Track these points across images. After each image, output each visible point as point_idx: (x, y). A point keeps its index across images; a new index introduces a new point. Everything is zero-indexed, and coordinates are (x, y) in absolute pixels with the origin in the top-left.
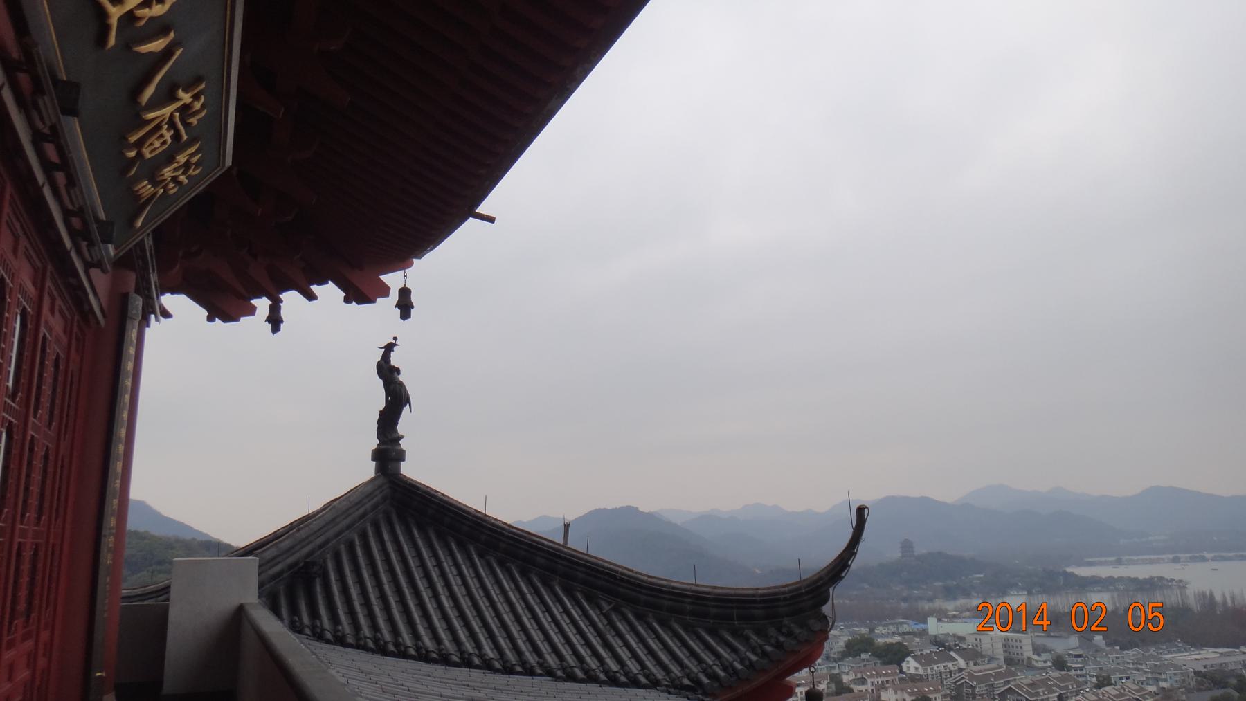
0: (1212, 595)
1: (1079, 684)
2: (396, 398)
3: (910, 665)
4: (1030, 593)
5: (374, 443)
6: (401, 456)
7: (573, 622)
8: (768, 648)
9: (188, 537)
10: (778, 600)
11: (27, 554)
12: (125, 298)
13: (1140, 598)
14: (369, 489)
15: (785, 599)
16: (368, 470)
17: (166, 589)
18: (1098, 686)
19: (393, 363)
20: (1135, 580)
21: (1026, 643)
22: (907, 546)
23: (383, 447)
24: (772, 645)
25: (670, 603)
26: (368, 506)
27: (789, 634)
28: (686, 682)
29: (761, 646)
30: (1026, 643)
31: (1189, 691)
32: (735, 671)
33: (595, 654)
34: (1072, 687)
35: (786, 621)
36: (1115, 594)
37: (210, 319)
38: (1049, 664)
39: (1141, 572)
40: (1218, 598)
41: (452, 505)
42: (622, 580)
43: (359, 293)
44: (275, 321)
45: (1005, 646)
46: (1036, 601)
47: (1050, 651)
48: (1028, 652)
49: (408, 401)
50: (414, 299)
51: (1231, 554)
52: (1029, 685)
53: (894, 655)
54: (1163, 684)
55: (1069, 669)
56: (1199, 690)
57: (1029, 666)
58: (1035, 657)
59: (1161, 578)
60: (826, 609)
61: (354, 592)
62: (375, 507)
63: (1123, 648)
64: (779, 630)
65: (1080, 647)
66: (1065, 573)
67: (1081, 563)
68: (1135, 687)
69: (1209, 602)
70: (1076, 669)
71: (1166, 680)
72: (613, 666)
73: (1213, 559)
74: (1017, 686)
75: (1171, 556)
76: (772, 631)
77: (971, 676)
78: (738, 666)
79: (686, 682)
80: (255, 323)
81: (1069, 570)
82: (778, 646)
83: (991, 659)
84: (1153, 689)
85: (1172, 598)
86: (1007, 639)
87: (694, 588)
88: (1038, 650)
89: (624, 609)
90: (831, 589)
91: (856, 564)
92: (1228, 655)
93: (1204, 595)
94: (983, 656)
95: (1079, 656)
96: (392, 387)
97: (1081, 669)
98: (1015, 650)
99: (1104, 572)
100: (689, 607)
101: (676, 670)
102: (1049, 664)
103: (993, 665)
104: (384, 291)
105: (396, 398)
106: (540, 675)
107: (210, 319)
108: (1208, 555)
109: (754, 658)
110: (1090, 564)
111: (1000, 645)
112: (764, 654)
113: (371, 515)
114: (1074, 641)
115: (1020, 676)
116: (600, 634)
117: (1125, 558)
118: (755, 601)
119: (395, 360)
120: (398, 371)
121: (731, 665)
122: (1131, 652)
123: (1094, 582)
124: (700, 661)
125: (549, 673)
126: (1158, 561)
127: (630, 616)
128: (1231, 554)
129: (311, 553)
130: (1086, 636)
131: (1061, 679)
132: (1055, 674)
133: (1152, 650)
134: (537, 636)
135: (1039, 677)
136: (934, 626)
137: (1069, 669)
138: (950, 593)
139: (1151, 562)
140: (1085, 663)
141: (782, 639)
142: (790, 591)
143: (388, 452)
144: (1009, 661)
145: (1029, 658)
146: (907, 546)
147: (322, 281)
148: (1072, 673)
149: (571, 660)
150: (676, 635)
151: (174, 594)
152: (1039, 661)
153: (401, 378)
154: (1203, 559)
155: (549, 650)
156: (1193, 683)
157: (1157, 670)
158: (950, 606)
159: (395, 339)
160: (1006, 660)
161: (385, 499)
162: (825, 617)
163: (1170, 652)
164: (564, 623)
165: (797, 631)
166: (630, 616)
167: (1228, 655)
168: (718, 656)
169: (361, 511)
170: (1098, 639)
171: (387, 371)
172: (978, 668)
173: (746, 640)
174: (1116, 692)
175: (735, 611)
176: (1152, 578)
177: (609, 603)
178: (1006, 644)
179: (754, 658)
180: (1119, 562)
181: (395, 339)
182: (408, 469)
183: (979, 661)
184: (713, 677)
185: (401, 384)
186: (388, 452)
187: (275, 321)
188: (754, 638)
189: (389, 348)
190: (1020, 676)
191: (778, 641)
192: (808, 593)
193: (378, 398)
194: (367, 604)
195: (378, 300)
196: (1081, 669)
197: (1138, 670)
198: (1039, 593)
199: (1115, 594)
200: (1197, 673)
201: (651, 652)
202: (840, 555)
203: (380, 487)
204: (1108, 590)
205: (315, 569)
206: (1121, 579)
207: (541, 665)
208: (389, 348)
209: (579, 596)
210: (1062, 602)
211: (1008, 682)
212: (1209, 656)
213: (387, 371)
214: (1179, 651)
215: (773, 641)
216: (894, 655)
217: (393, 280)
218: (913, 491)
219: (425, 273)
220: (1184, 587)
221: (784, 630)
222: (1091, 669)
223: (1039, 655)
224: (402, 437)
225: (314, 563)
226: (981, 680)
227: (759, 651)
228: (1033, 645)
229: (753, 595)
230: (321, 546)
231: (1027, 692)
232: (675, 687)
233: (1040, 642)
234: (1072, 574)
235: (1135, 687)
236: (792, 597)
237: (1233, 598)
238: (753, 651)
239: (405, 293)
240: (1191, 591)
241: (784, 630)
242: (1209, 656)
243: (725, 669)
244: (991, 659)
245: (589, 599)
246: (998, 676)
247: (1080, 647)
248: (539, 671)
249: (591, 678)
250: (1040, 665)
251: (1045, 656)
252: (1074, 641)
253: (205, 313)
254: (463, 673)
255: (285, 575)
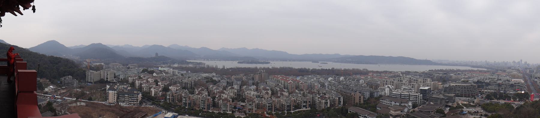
3: (155, 74)
22: (157, 54)
39: (198, 61)
48: (177, 73)
53: (152, 72)
57: (177, 75)
85: (203, 66)
99: (192, 61)
123: (190, 62)
130: (187, 71)
136: (160, 69)
138: (164, 63)
146: (157, 54)
157: (198, 76)
158: (164, 66)
210: (184, 66)
212: (207, 75)
216: (152, 72)
217: (32, 4)
218: (50, 40)
239: (34, 7)
242: (207, 75)
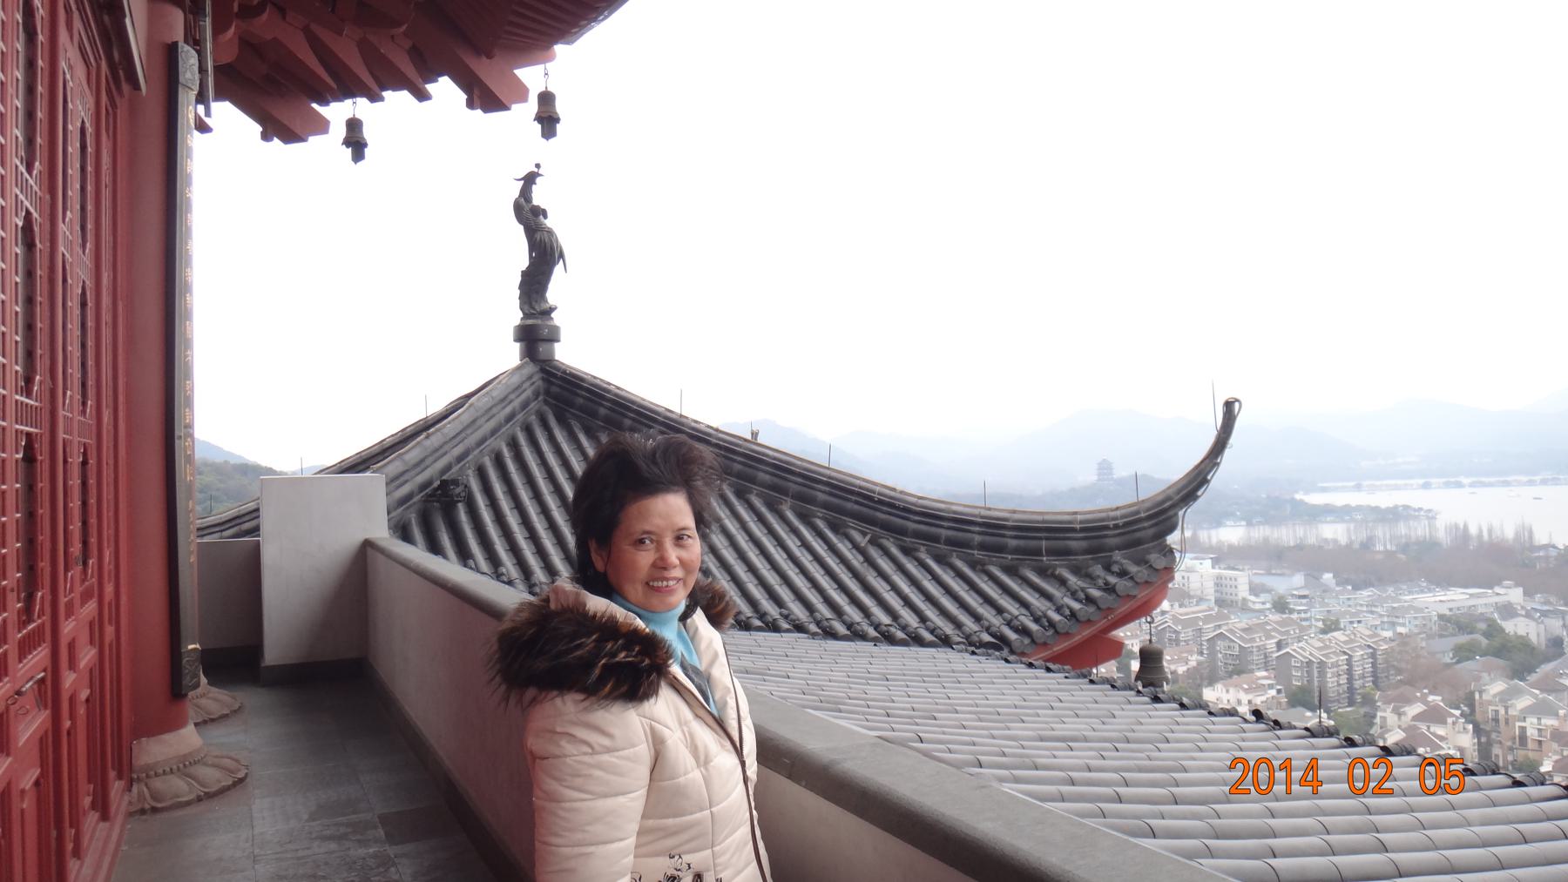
0: (1466, 526)
1: (1302, 629)
2: (544, 256)
4: (1250, 524)
5: (516, 317)
6: (553, 337)
7: (817, 559)
8: (1095, 593)
9: (219, 459)
10: (1106, 528)
11: (76, 460)
12: (171, 52)
13: (1381, 532)
14: (516, 380)
15: (1116, 527)
16: (509, 356)
17: (257, 510)
18: (1324, 632)
19: (535, 202)
20: (1376, 509)
21: (1241, 581)
23: (530, 322)
24: (1099, 588)
25: (950, 533)
26: (517, 403)
27: (1123, 574)
28: (986, 638)
29: (1083, 590)
30: (1241, 581)
31: (1430, 637)
32: (1052, 624)
33: (854, 601)
34: (1293, 631)
35: (1117, 556)
36: (1352, 526)
37: (266, 136)
38: (1268, 606)
40: (1473, 531)
41: (633, 402)
42: (881, 502)
43: (485, 98)
44: (355, 142)
45: (1217, 585)
46: (1260, 533)
47: (1269, 591)
48: (1243, 592)
49: (561, 256)
50: (560, 107)
51: (1492, 480)
52: (1244, 630)
54: (1400, 629)
55: (1291, 611)
56: (1441, 636)
57: (1244, 607)
58: (1252, 598)
59: (1406, 507)
60: (1173, 539)
61: (513, 520)
62: (525, 405)
63: (1356, 588)
64: (1107, 568)
65: (1305, 587)
66: (1293, 499)
67: (1307, 492)
68: (1368, 632)
69: (1462, 536)
70: (1299, 612)
71: (1403, 625)
72: (885, 619)
73: (1472, 485)
74: (1231, 631)
75: (1421, 481)
76: (1098, 570)
77: (1175, 619)
78: (1056, 617)
79: (986, 638)
80: (327, 147)
81: (1298, 497)
82: (1109, 589)
83: (1201, 600)
84: (1388, 634)
85: (1419, 530)
86: (1219, 577)
87: (984, 512)
88: (1255, 590)
89: (885, 542)
90: (1181, 513)
91: (1220, 479)
92: (1478, 596)
93: (1456, 526)
94: (1190, 597)
95: (1304, 597)
96: (538, 236)
97: (1305, 612)
98: (1229, 590)
99: (1338, 499)
100: (978, 538)
101: (969, 624)
102: (1268, 606)
103: (1203, 606)
104: (521, 93)
105: (544, 256)
106: (788, 631)
107: (266, 136)
108: (1466, 481)
109: (1076, 606)
110: (1324, 490)
111: (1211, 584)
112: (1090, 600)
113: (520, 417)
114: (1298, 580)
115: (1234, 619)
116: (856, 575)
117: (1365, 483)
118: (1073, 530)
119: (539, 197)
120: (544, 213)
121: (1045, 616)
122: (1365, 593)
123: (1328, 511)
124: (1000, 611)
125: (799, 628)
126: (1405, 487)
127: (895, 551)
128: (1492, 480)
129: (448, 468)
130: (1313, 575)
131: (1282, 623)
132: (1274, 617)
133: (1390, 589)
134: (772, 578)
135: (1255, 621)
137: (1291, 611)
139: (1397, 488)
140: (1311, 605)
141: (1112, 580)
142: (1123, 517)
143: (535, 335)
144: (1220, 602)
145: (1244, 599)
146: (1105, 468)
147: (432, 79)
148: (1295, 616)
149: (824, 611)
150: (960, 575)
151: (267, 523)
152: (1259, 602)
153: (549, 223)
154: (1459, 485)
155: (792, 597)
156: (1435, 628)
159: (538, 166)
160: (1217, 601)
161: (536, 394)
162: (1171, 551)
163: (1410, 593)
164: (803, 556)
165: (1133, 569)
166: (895, 551)
167: (1478, 596)
168: (1024, 604)
169: (508, 410)
170: (1328, 577)
171: (529, 215)
172: (1183, 610)
173: (1063, 582)
174: (1344, 638)
175: (1044, 543)
176: (1396, 507)
177: (864, 534)
178: (1218, 585)
179: (1076, 606)
180: (1358, 487)
181: (538, 166)
182: (569, 353)
183: (1186, 601)
184: (1023, 631)
185: (550, 232)
186: (535, 335)
187: (355, 142)
188: (1073, 580)
189: (530, 180)
190: (1234, 619)
191: (1107, 583)
192: (1150, 517)
193: (519, 256)
194: (533, 537)
195: (515, 107)
196: (1305, 612)
197: (1372, 612)
198: (1260, 523)
199: (1352, 526)
200: (1441, 617)
201: (929, 598)
202: (1197, 467)
203: (530, 378)
204: (1343, 521)
205: (458, 490)
206: (1359, 508)
207: (786, 617)
208: (530, 180)
209: (821, 524)
210: (1286, 535)
211: (1219, 626)
212: (1457, 598)
213: (529, 215)
214: (1422, 592)
215: (1101, 582)
217: (531, 76)
219: (568, 67)
220: (1434, 518)
221: (1115, 568)
222: (1317, 612)
223: (1256, 595)
224: (552, 309)
225: (455, 482)
226: (1187, 623)
227: (1082, 596)
228: (1250, 583)
229: (1070, 522)
230: (460, 459)
231: (1241, 638)
232: (971, 644)
233: (1257, 580)
234: (1302, 502)
235: (1368, 632)
236: (1126, 524)
237: (1490, 531)
238: (1074, 595)
239: (546, 99)
240: (1441, 524)
241: (1115, 568)
242: (1457, 598)
243: (1037, 620)
244: (1201, 600)
245: (835, 528)
246: (1207, 619)
247: (1305, 587)
248: (785, 626)
249: (856, 635)
250: (1258, 606)
251: (1264, 597)
252: (1298, 580)
253: (259, 129)
254: (942, 654)
255: (416, 499)
